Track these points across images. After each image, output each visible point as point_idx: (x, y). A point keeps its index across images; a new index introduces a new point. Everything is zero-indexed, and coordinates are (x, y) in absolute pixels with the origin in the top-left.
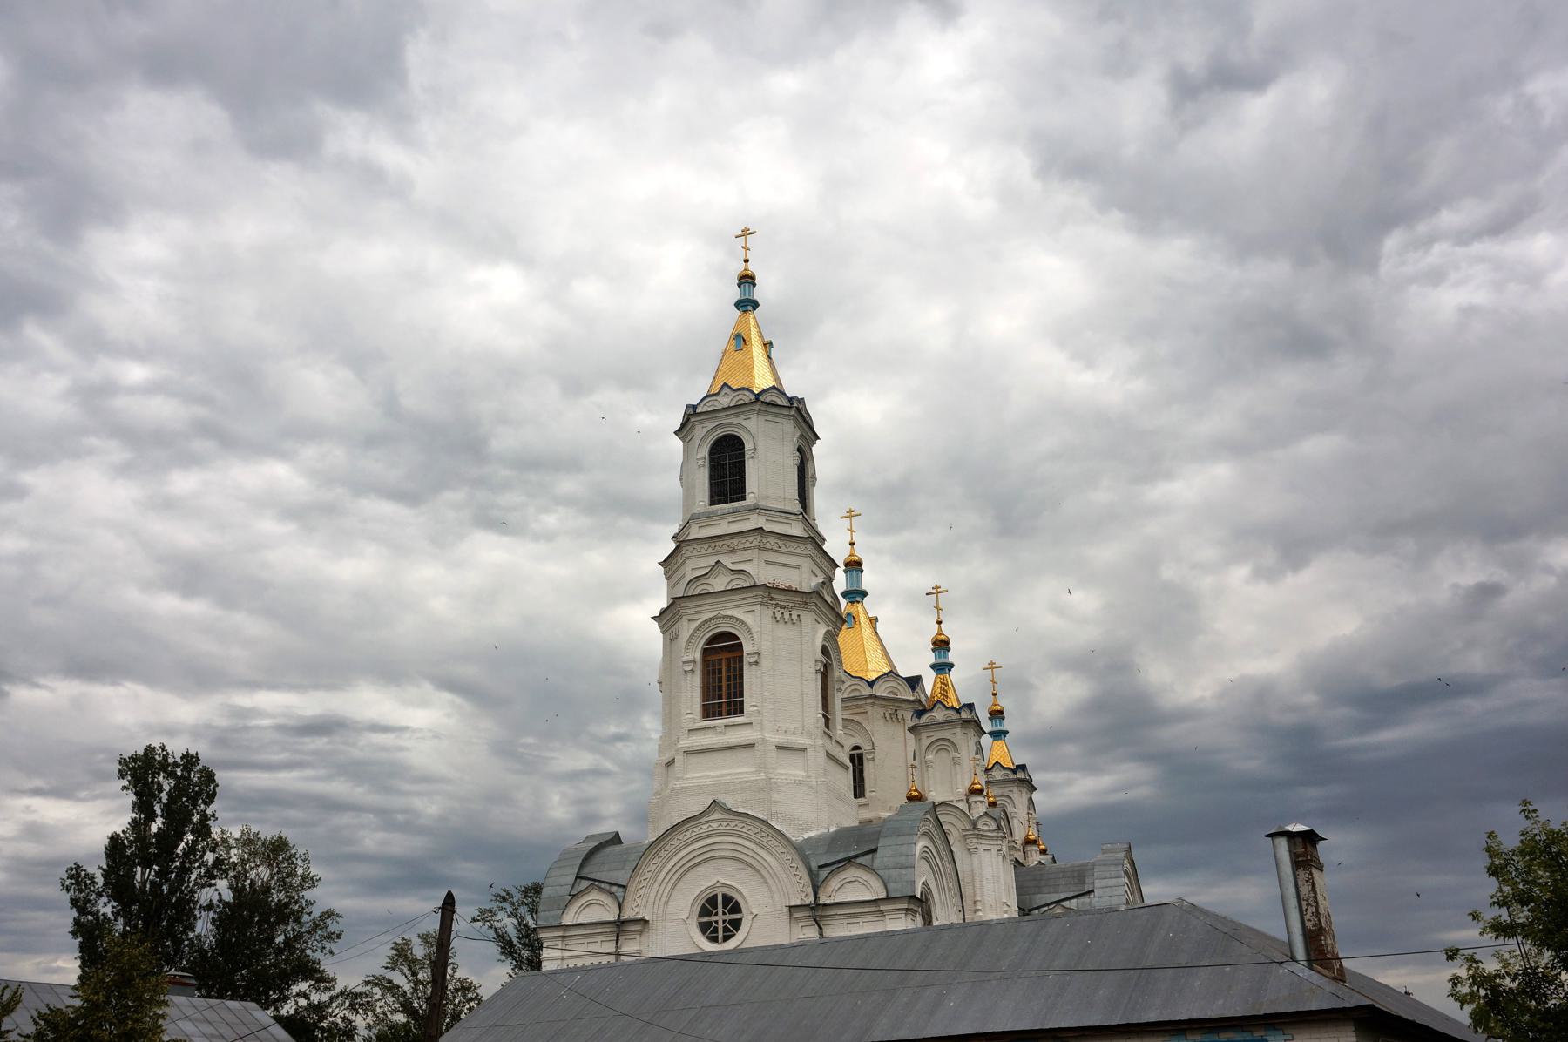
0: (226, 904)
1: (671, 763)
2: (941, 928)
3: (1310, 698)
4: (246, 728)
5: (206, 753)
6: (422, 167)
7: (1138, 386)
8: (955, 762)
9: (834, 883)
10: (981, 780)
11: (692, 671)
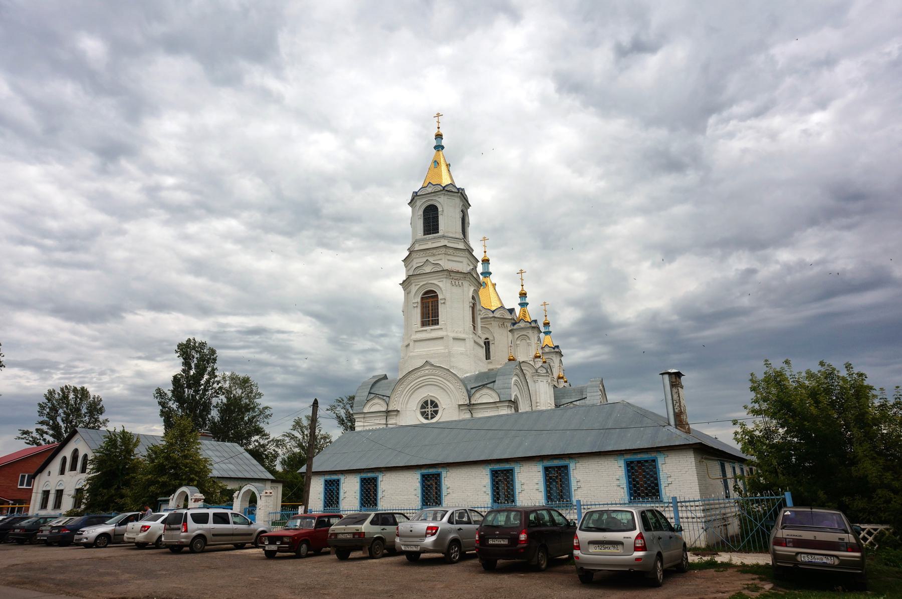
0: (225, 404)
1: (408, 345)
2: (522, 413)
3: (675, 317)
4: (225, 332)
5: (210, 343)
6: (287, 90)
7: (602, 184)
8: (529, 344)
9: (478, 395)
10: (540, 352)
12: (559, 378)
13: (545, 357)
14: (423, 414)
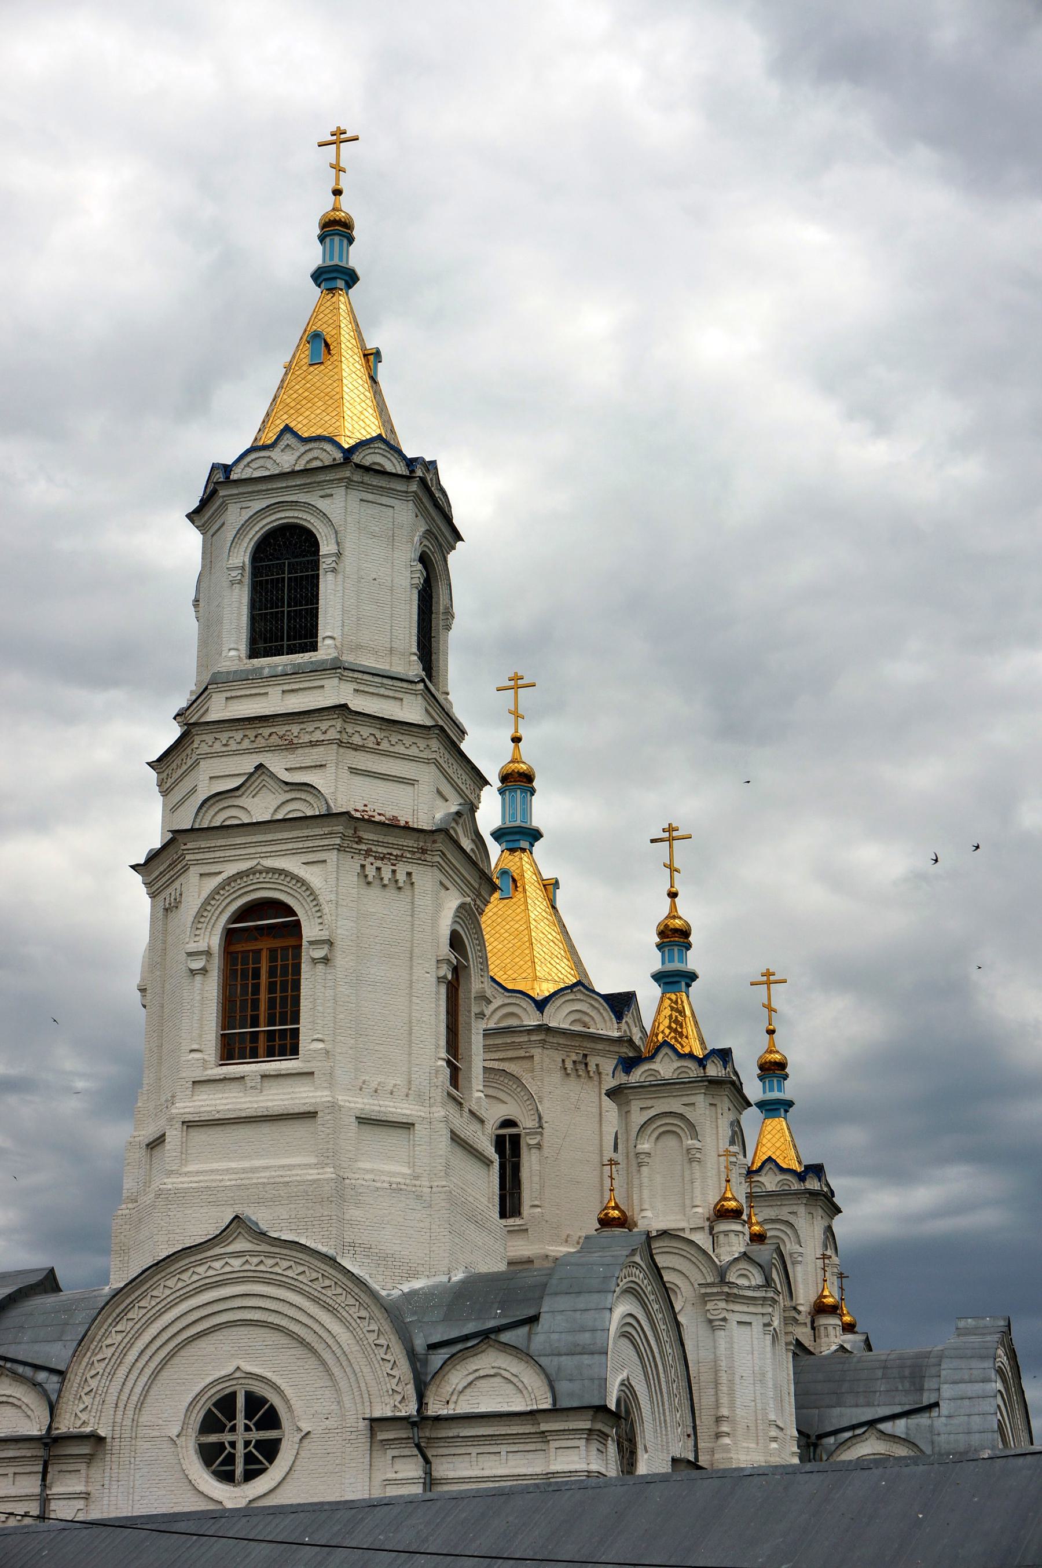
1: (156, 1143)
7: (970, 470)
8: (692, 1157)
9: (457, 1378)
10: (738, 1193)
11: (204, 971)
12: (821, 1309)
13: (761, 1214)
14: (209, 1455)
